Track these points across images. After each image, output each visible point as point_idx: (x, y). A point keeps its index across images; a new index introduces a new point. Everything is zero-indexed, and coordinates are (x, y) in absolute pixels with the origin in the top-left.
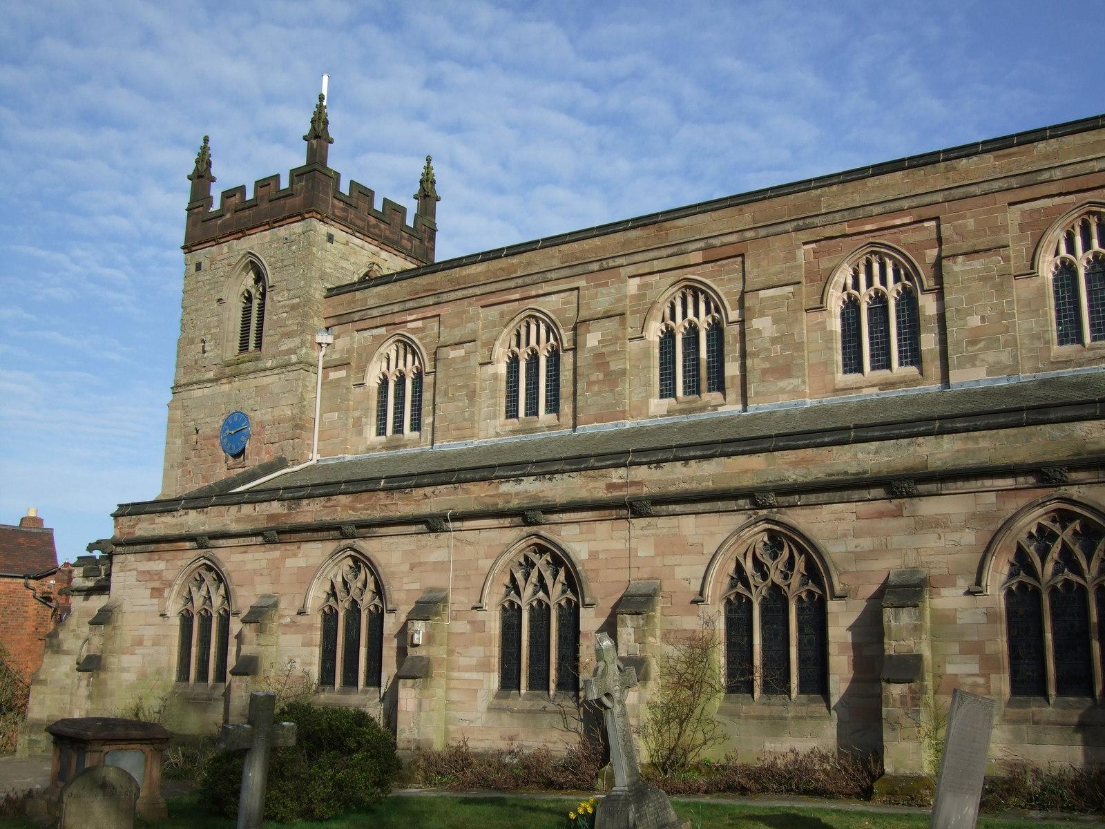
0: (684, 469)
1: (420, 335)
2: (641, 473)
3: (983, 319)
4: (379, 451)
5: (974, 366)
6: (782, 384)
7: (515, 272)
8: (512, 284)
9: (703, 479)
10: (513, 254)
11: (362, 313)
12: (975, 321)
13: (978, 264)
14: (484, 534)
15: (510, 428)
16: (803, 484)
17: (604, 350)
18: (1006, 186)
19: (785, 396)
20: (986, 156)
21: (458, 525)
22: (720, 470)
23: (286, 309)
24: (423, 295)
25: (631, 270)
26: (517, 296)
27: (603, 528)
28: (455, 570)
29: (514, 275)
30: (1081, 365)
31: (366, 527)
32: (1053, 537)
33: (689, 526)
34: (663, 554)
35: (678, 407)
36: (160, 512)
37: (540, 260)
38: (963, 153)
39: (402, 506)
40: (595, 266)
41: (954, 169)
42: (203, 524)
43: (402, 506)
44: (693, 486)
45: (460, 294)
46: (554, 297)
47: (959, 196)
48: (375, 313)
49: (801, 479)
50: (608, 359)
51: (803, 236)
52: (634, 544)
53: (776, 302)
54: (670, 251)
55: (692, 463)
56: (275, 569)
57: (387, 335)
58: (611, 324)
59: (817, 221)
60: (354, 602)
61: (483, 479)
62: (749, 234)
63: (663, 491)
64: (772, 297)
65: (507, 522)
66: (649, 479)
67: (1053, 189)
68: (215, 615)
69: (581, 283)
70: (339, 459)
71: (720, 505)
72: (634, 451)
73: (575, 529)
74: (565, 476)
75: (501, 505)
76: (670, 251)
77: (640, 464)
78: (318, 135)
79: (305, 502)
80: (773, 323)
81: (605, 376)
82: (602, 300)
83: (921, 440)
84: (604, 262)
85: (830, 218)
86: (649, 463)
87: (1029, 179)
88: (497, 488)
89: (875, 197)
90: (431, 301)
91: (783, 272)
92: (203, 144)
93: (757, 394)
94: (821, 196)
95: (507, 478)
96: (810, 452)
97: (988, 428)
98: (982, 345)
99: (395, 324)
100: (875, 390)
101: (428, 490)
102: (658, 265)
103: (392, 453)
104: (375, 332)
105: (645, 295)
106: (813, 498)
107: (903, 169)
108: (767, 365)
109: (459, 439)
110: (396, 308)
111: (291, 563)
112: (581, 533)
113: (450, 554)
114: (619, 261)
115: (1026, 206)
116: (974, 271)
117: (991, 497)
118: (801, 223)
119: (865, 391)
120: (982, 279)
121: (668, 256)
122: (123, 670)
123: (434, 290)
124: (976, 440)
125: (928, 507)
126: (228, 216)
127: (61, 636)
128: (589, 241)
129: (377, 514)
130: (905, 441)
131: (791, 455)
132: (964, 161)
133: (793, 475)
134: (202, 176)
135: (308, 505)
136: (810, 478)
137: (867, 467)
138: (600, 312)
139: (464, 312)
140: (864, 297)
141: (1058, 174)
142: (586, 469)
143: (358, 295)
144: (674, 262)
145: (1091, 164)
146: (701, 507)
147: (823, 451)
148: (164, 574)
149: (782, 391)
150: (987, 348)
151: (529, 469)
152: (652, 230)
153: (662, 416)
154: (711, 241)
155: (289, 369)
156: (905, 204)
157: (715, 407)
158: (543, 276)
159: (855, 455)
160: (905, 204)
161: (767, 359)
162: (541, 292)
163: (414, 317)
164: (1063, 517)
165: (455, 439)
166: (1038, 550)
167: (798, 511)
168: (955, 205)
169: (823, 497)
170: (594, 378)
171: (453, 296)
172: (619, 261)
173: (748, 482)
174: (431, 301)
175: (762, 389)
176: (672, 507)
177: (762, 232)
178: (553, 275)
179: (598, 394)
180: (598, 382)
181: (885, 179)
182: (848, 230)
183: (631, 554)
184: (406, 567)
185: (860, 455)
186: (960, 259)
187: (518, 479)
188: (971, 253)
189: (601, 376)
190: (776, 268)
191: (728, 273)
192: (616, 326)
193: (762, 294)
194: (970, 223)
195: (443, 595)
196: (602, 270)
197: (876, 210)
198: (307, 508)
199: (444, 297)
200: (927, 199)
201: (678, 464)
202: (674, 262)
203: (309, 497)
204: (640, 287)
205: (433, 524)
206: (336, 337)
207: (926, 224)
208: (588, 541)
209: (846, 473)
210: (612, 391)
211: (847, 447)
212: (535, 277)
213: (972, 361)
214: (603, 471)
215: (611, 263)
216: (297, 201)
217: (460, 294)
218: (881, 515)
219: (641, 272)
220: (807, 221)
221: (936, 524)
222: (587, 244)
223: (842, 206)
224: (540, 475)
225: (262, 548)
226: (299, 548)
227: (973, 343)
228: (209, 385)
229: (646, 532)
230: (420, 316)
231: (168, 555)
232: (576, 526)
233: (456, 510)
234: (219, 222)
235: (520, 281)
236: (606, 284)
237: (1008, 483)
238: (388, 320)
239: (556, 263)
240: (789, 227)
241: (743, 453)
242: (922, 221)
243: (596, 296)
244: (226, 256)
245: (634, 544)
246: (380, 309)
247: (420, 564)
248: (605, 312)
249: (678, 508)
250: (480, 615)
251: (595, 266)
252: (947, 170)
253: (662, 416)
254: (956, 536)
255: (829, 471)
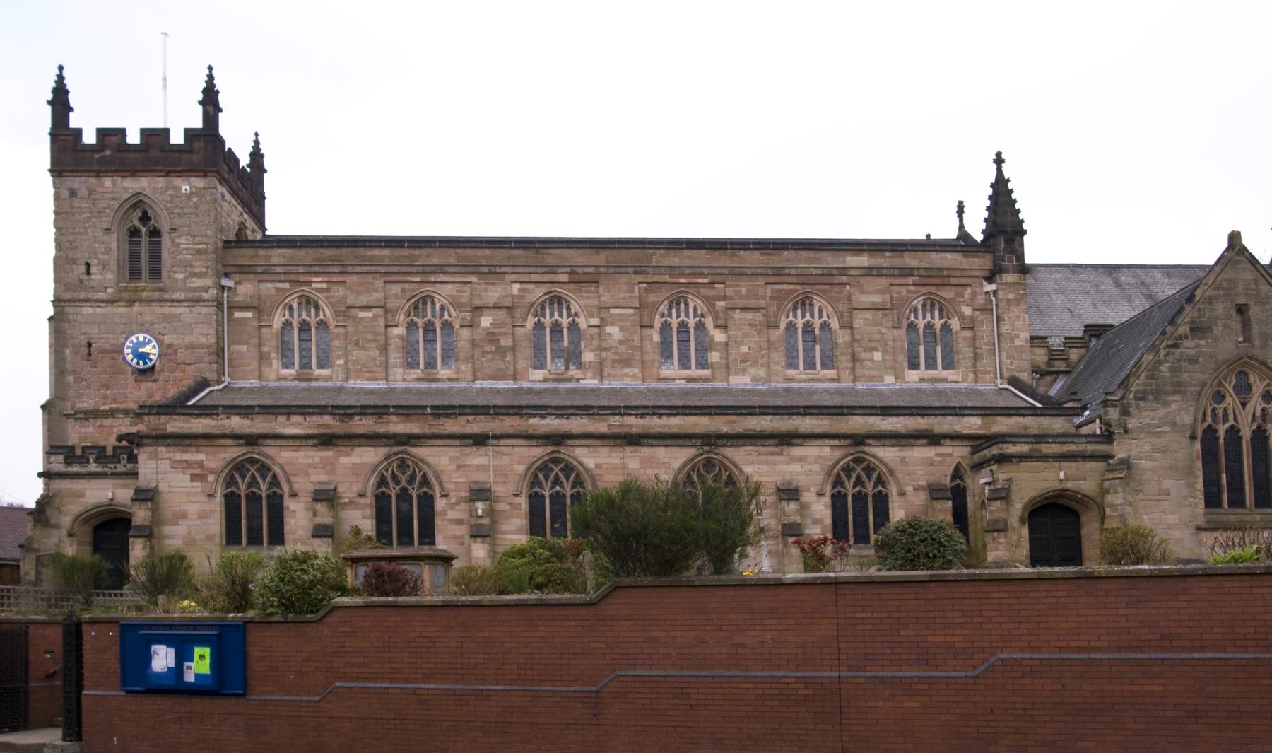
0: (659, 420)
1: (326, 295)
2: (631, 420)
3: (750, 348)
4: (291, 381)
5: (744, 375)
6: (626, 371)
7: (417, 261)
8: (414, 269)
9: (671, 426)
10: (415, 247)
11: (266, 268)
12: (744, 349)
13: (749, 316)
14: (515, 449)
15: (415, 376)
16: (731, 434)
17: (496, 330)
18: (764, 272)
19: (628, 379)
20: (755, 252)
21: (495, 442)
22: (682, 422)
23: (193, 252)
24: (330, 263)
25: (514, 277)
26: (418, 279)
27: (604, 451)
28: (494, 471)
29: (416, 263)
30: (800, 382)
31: (410, 439)
32: (853, 469)
33: (661, 453)
34: (645, 468)
35: (551, 377)
36: (197, 415)
37: (436, 258)
38: (741, 247)
39: (450, 426)
40: (486, 270)
41: (736, 256)
42: (250, 427)
43: (450, 426)
44: (666, 430)
45: (365, 269)
46: (449, 286)
47: (738, 273)
48: (279, 270)
49: (730, 432)
50: (499, 337)
51: (640, 278)
52: (626, 461)
53: (622, 318)
54: (544, 270)
55: (664, 417)
56: (329, 466)
57: (290, 290)
58: (501, 314)
59: (649, 270)
60: (404, 490)
61: (516, 414)
62: (602, 270)
63: (646, 431)
64: (619, 315)
65: (534, 443)
66: (636, 424)
67: (790, 279)
68: (243, 495)
69: (474, 279)
70: (252, 383)
71: (680, 442)
72: (624, 407)
73: (585, 450)
74: (578, 418)
75: (531, 432)
76: (544, 270)
77: (630, 415)
78: (210, 99)
79: (357, 418)
80: (620, 331)
81: (497, 348)
82: (493, 294)
83: (794, 417)
84: (492, 268)
85: (657, 270)
86: (636, 415)
87: (778, 271)
88: (527, 421)
89: (687, 262)
90: (337, 270)
91: (625, 299)
92: (58, 72)
93: (609, 375)
94: (652, 254)
95: (535, 415)
96: (734, 418)
97: (828, 414)
98: (749, 363)
99: (299, 281)
100: (684, 382)
101: (471, 418)
102: (534, 278)
103: (304, 384)
104: (279, 285)
105: (524, 297)
106: (735, 442)
107: (705, 249)
108: (616, 357)
109: (372, 380)
110: (301, 270)
111: (343, 460)
112: (589, 452)
113: (489, 459)
114: (504, 269)
115: (776, 287)
116: (745, 320)
117: (828, 449)
118: (638, 269)
119: (677, 382)
120: (749, 325)
121: (543, 273)
122: (172, 537)
123: (339, 261)
124: (822, 419)
125: (797, 451)
126: (108, 153)
127: (48, 512)
128: (481, 250)
129: (427, 431)
130: (786, 417)
131: (724, 418)
132: (742, 252)
133: (725, 429)
134: (60, 101)
135: (361, 420)
136: (735, 431)
137: (766, 428)
138: (489, 303)
139: (369, 283)
140: (674, 322)
141: (793, 272)
142: (593, 414)
143: (261, 252)
144: (547, 278)
145: (811, 270)
146: (669, 442)
147: (742, 418)
148: (205, 463)
149: (626, 375)
150: (751, 365)
151: (549, 411)
152: (531, 253)
153: (540, 381)
154: (574, 269)
155: (201, 303)
156: (706, 271)
157: (578, 380)
158: (441, 269)
159: (760, 422)
160: (706, 271)
161: (616, 353)
162: (439, 280)
163: (320, 279)
164: (858, 461)
165: (368, 380)
166: (544, 476)
167: (727, 449)
168: (735, 278)
169: (741, 442)
170: (488, 348)
171: (358, 269)
172: (504, 269)
173: (698, 430)
174: (337, 270)
175: (613, 372)
176: (650, 441)
177: (611, 270)
178: (451, 270)
179: (492, 360)
180: (492, 352)
181: (695, 253)
182: (669, 280)
183: (624, 466)
184: (453, 467)
185: (762, 422)
186: (738, 311)
187: (543, 417)
188: (745, 309)
189: (493, 349)
190: (621, 295)
191: (587, 292)
192: (505, 315)
193: (612, 311)
194: (744, 290)
195: (488, 486)
196: (490, 273)
197: (687, 271)
198: (359, 422)
199: (350, 269)
200: (718, 271)
201: (655, 417)
202: (547, 278)
203: (360, 414)
204: (520, 290)
205: (480, 440)
206: (236, 283)
207: (716, 286)
208: (595, 457)
209: (755, 430)
210: (503, 360)
211: (755, 417)
212: (434, 268)
213: (743, 371)
214: (605, 417)
215: (498, 270)
216: (196, 158)
217: (365, 269)
218: (772, 454)
219: (521, 280)
220: (643, 269)
221: (802, 459)
222: (478, 252)
223: (666, 263)
224: (560, 416)
225: (315, 449)
226: (352, 450)
227: (743, 361)
228: (103, 305)
229: (633, 454)
230: (326, 279)
231: (209, 449)
232: (586, 448)
233: (495, 433)
234: (97, 156)
235: (420, 269)
236: (494, 284)
237: (836, 442)
238: (292, 277)
239: (452, 261)
240: (631, 270)
241: (696, 414)
242: (714, 283)
243: (486, 290)
244: (110, 190)
245: (626, 461)
246: (284, 268)
247: (465, 466)
248: (494, 304)
249: (654, 442)
250: (517, 500)
251: (486, 270)
252: (732, 255)
253: (540, 381)
254: (811, 466)
255: (745, 428)
